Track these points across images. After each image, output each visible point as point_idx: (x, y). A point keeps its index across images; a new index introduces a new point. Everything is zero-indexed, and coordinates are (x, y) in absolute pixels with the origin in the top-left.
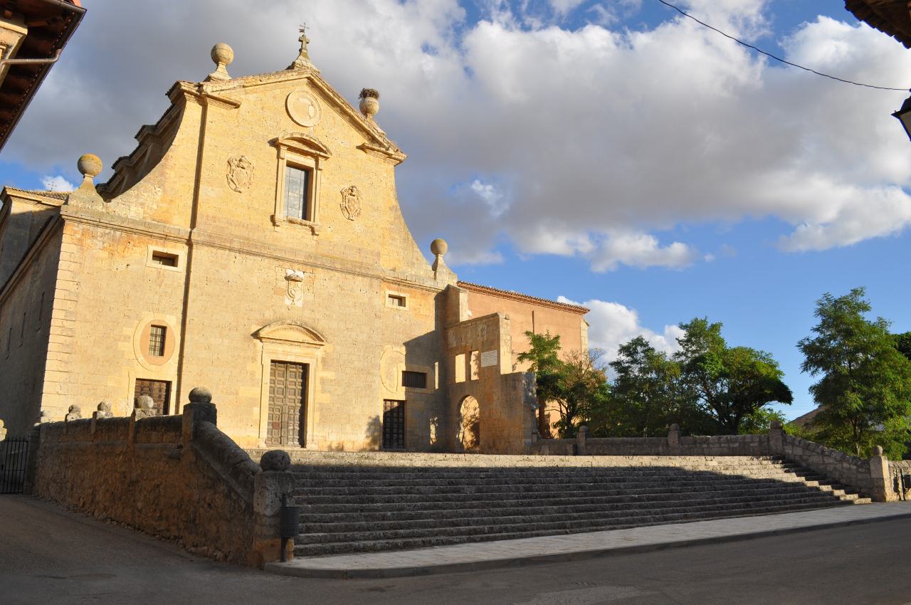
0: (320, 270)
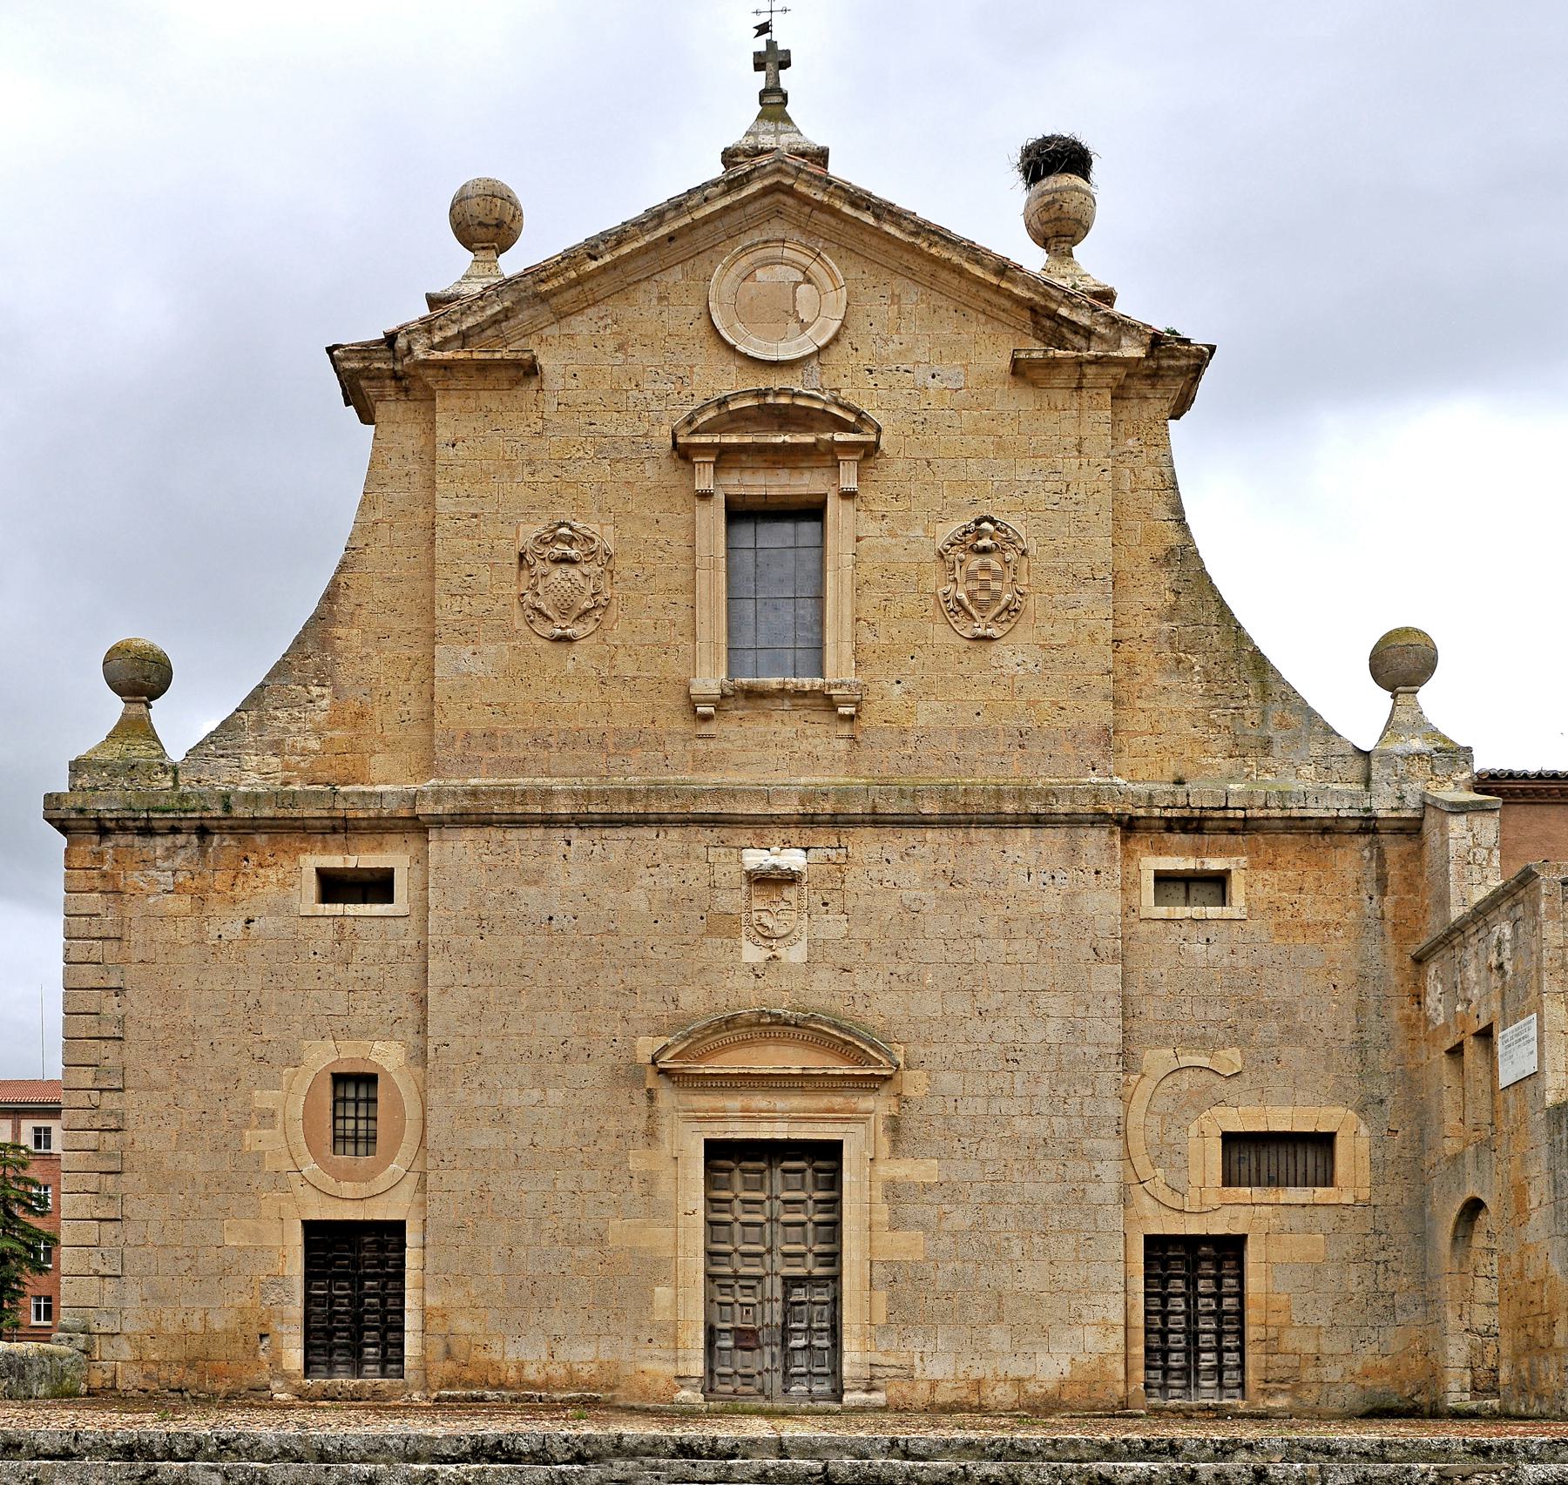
0: (867, 833)
